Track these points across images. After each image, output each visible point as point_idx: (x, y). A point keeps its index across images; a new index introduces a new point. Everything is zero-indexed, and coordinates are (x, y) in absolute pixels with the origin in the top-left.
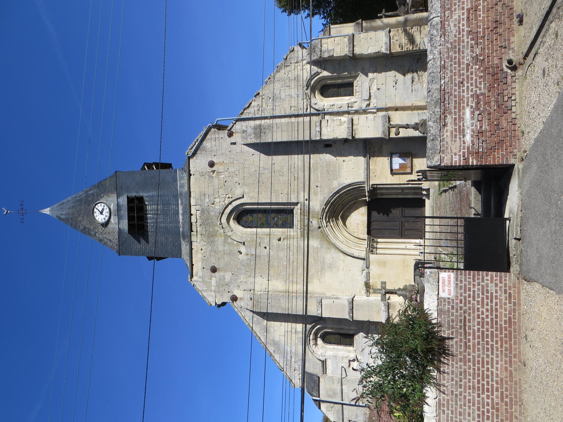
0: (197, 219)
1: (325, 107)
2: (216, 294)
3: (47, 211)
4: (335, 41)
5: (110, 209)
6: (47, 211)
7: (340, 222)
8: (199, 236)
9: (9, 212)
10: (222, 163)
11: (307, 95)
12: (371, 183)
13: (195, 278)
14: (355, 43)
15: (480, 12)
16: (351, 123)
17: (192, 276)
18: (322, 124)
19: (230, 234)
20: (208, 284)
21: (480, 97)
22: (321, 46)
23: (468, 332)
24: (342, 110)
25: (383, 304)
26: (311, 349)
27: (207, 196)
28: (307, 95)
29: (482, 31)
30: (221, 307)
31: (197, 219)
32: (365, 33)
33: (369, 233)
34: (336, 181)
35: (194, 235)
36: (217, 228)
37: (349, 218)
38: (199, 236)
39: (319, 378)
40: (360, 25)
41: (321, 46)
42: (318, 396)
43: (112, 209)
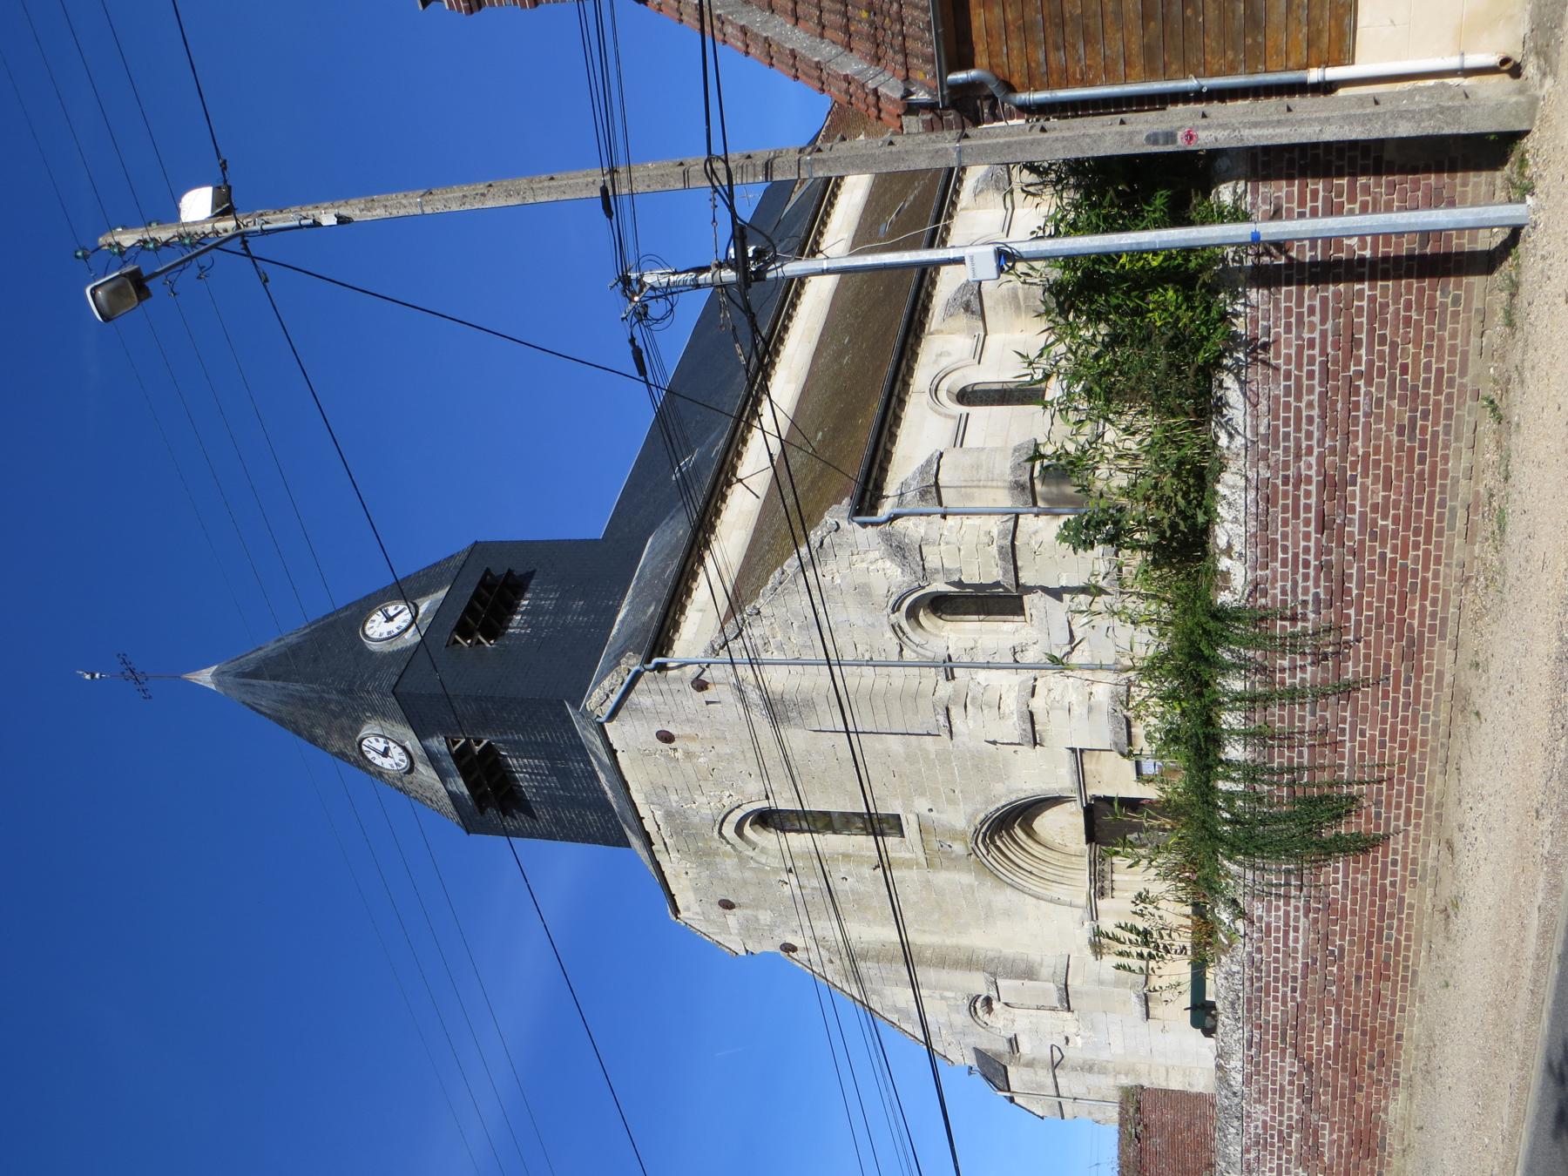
0: (658, 826)
1: (951, 651)
2: (746, 941)
3: (205, 677)
4: (962, 552)
5: (405, 749)
6: (205, 677)
7: (1018, 831)
8: (674, 854)
9: (97, 676)
10: (694, 738)
11: (897, 629)
12: (1090, 793)
13: (683, 915)
14: (1019, 564)
15: (1362, 300)
16: (1028, 720)
17: (676, 911)
18: (953, 713)
19: (751, 853)
20: (725, 928)
21: (1357, 383)
22: (922, 560)
23: (1306, 475)
24: (997, 659)
25: (1133, 995)
26: (980, 1022)
27: (671, 791)
28: (897, 629)
29: (1368, 306)
30: (630, 348)
31: (658, 826)
32: (1046, 513)
33: (1091, 837)
34: (1000, 784)
35: (659, 851)
36: (714, 845)
37: (1039, 818)
38: (674, 854)
39: (1005, 1068)
40: (1028, 491)
41: (922, 560)
42: (1006, 1088)
43: (410, 748)
